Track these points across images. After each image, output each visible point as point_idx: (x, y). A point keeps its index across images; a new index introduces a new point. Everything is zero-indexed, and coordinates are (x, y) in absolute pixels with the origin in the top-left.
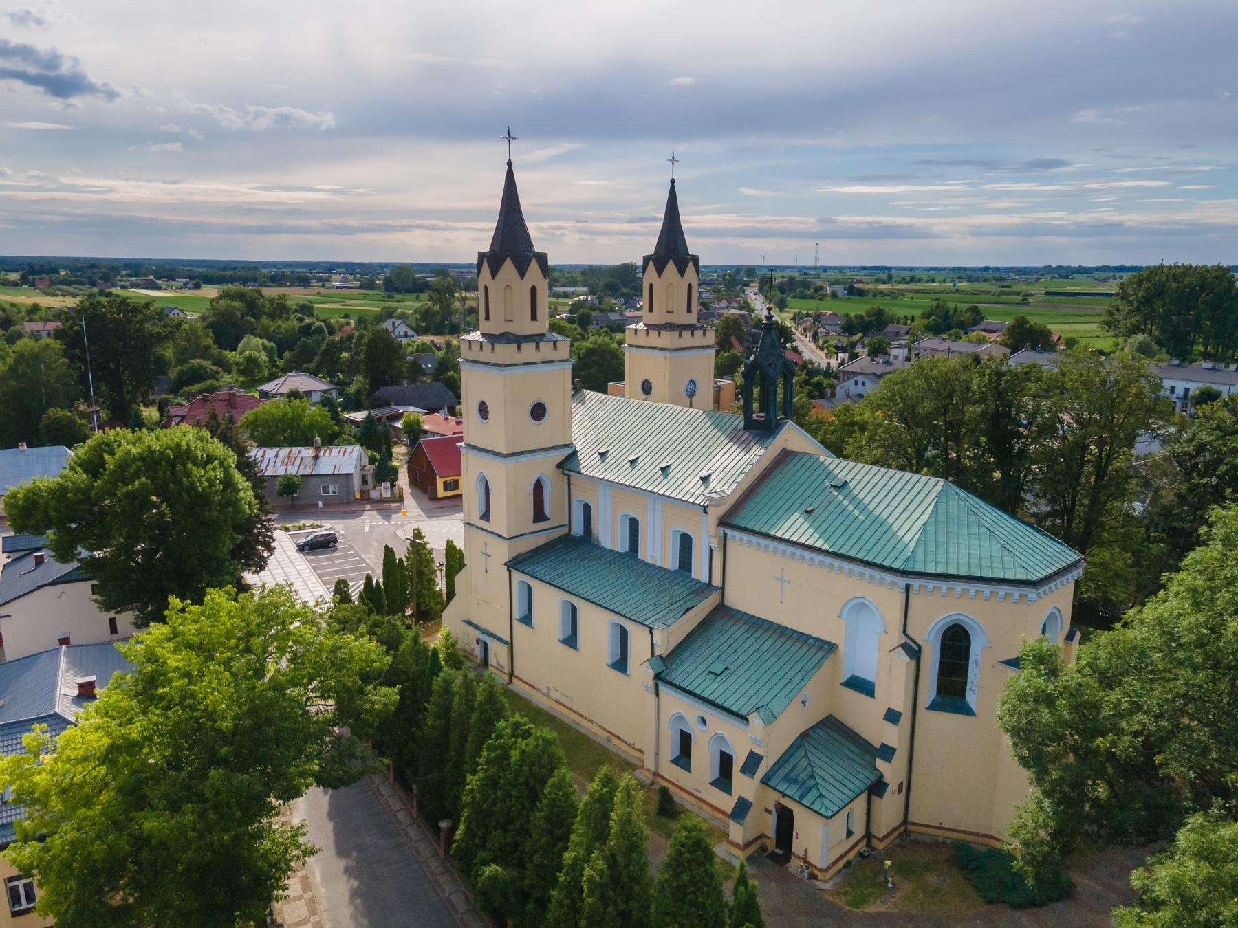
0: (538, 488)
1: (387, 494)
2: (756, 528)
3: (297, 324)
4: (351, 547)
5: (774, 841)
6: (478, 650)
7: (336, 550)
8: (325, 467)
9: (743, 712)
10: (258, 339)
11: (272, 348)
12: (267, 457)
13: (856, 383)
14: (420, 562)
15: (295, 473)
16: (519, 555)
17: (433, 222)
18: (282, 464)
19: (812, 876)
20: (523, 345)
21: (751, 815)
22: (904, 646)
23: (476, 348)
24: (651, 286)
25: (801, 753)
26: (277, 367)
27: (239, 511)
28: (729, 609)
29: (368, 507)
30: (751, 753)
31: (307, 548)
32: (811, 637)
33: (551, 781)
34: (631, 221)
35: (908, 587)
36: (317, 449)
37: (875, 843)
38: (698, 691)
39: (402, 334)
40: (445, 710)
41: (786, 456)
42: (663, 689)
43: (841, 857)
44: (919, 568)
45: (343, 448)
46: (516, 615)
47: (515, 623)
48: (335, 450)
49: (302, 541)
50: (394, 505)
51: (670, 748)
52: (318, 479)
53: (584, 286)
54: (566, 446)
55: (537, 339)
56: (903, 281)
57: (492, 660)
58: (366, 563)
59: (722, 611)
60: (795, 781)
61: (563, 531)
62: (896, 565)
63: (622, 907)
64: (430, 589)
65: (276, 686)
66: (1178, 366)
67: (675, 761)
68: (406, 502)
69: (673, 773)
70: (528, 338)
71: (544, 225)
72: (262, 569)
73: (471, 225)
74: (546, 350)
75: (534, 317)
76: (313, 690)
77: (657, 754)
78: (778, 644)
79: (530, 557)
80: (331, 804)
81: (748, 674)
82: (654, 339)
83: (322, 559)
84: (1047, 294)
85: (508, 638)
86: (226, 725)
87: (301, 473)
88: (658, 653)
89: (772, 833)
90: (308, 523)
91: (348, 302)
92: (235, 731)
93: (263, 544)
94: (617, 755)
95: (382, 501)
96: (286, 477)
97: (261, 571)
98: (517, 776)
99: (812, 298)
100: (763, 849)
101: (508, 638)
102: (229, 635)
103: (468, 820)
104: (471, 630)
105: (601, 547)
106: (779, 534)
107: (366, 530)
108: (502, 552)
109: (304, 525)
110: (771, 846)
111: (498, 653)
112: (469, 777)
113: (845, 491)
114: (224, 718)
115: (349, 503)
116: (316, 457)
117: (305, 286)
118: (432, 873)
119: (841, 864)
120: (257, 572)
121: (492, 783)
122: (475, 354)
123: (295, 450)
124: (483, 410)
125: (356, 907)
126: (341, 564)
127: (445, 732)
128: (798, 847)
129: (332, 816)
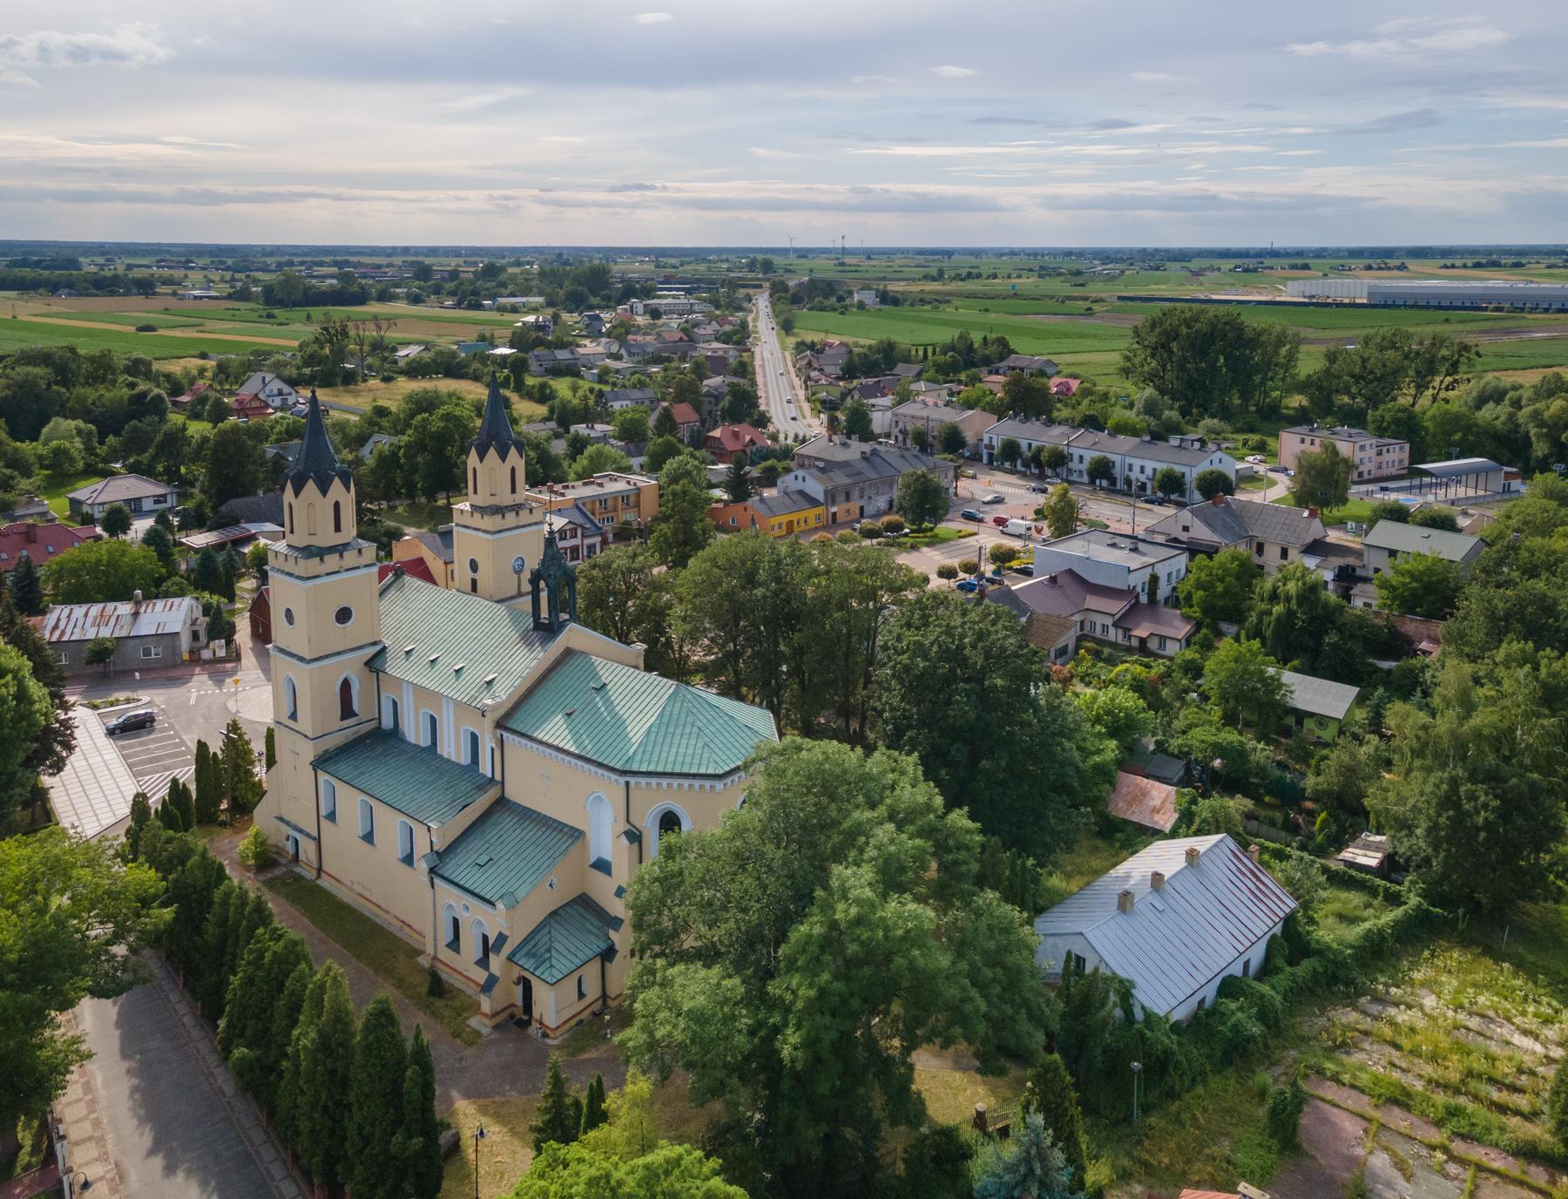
0: (346, 686)
1: (222, 653)
2: (524, 731)
3: (125, 392)
4: (172, 727)
5: (521, 1011)
6: (290, 847)
7: (153, 731)
8: (146, 626)
9: (493, 900)
10: (69, 421)
11: (90, 433)
12: (74, 617)
13: (796, 478)
14: (238, 755)
15: (108, 636)
16: (326, 752)
17: (336, 190)
18: (93, 625)
19: (545, 1035)
20: (326, 557)
21: (497, 989)
22: (628, 834)
23: (281, 558)
24: (475, 469)
25: (546, 930)
26: (97, 455)
27: (33, 724)
28: (508, 801)
29: (197, 670)
30: (500, 933)
31: (118, 731)
32: (566, 825)
33: (292, 975)
34: (613, 189)
35: (627, 784)
36: (138, 603)
37: (609, 1002)
38: (461, 883)
39: (275, 392)
40: (223, 922)
41: (568, 653)
42: (437, 881)
43: (574, 1016)
44: (635, 767)
45: (170, 601)
46: (323, 812)
47: (322, 819)
48: (160, 604)
49: (113, 722)
50: (229, 666)
51: (446, 935)
52: (137, 641)
53: (541, 295)
54: (375, 644)
55: (340, 549)
56: (958, 278)
57: (302, 856)
58: (187, 747)
59: (502, 803)
60: (534, 956)
61: (373, 724)
62: (617, 767)
63: (329, 1065)
64: (246, 781)
65: (60, 922)
66: (1149, 442)
67: (448, 946)
68: (243, 662)
69: (446, 955)
70: (332, 549)
71: (496, 193)
72: (60, 770)
73: (392, 193)
74: (350, 558)
75: (338, 528)
76: (95, 916)
77: (435, 940)
78: (540, 833)
79: (337, 755)
80: (119, 1014)
81: (507, 864)
82: (477, 521)
83: (134, 743)
84: (1120, 298)
85: (315, 834)
86: (13, 957)
87: (116, 635)
88: (435, 848)
89: (520, 1002)
90: (122, 696)
91: (209, 325)
92: (21, 960)
93: (61, 743)
94: (407, 943)
95: (216, 661)
96: (96, 641)
97: (59, 772)
98: (269, 974)
99: (834, 310)
100: (512, 1016)
101: (315, 834)
102: (17, 880)
103: (231, 1014)
104: (283, 827)
105: (406, 742)
106: (540, 737)
107: (192, 702)
108: (309, 752)
109: (117, 700)
110: (519, 1014)
111: (307, 849)
112: (232, 978)
113: (602, 693)
114: (10, 951)
115: (175, 666)
116: (136, 615)
117: (146, 294)
118: (208, 1067)
119: (573, 1022)
120: (53, 775)
121: (249, 981)
122: (280, 563)
123: (110, 606)
124: (289, 615)
125: (135, 1101)
126: (157, 748)
127: (223, 940)
128: (536, 1014)
129: (119, 1024)
